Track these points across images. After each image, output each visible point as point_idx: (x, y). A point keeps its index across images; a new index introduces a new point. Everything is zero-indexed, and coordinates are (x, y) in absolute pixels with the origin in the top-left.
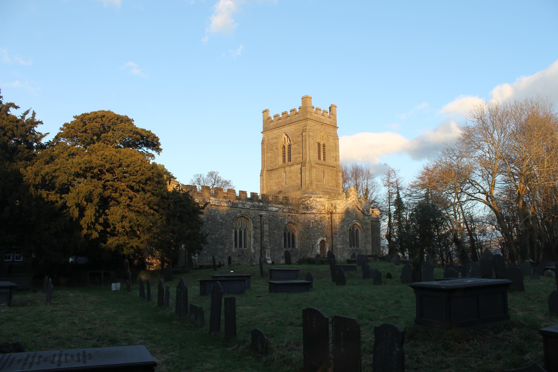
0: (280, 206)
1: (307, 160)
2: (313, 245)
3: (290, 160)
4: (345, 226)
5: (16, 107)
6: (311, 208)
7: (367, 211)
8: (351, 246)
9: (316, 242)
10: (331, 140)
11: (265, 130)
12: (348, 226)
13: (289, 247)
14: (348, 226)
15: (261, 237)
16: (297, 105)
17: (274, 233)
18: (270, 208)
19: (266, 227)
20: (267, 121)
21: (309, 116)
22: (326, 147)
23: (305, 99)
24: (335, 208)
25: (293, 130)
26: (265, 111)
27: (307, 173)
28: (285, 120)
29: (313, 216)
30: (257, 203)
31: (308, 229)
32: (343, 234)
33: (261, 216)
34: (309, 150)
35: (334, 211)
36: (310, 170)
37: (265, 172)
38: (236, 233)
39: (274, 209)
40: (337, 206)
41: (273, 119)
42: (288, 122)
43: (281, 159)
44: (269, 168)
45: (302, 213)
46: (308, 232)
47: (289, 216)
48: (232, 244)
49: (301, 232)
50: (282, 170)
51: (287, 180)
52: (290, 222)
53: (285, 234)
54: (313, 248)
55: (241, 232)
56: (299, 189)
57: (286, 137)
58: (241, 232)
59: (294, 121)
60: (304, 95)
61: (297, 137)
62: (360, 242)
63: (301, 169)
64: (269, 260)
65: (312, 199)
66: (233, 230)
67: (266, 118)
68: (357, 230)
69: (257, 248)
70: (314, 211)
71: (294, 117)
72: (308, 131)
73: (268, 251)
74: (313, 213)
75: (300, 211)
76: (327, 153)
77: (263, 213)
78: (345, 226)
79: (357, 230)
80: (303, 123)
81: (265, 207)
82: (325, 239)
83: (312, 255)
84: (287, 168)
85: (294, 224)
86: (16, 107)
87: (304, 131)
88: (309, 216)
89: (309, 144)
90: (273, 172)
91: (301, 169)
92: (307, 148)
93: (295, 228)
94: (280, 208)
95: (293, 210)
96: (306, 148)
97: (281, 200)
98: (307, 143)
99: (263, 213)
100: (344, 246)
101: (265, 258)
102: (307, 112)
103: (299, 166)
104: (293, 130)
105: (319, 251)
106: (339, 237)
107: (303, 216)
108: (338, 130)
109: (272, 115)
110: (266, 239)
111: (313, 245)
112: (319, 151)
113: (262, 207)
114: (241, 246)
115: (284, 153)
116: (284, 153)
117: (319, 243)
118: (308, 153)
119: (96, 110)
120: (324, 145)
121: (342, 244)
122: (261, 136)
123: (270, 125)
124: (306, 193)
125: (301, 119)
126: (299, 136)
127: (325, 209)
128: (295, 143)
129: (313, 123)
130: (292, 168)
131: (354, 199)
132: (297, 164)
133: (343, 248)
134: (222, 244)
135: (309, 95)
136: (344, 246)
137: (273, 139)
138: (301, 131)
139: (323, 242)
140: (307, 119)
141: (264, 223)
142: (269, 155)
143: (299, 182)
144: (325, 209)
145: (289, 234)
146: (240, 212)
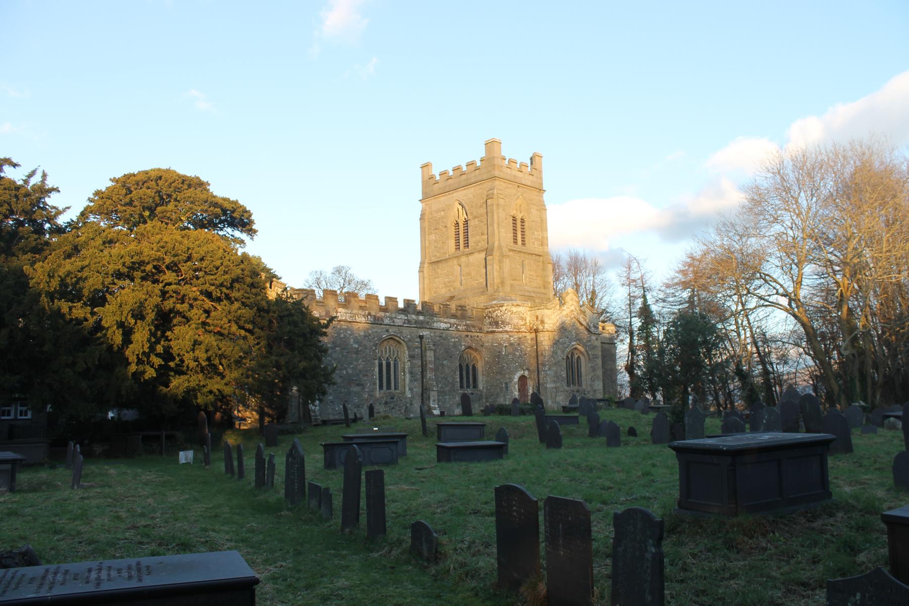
0: (453, 321)
1: (496, 245)
2: (506, 384)
3: (467, 245)
4: (559, 352)
5: (15, 166)
6: (503, 322)
7: (594, 326)
8: (568, 385)
9: (511, 379)
10: (534, 211)
11: (427, 196)
12: (563, 352)
13: (468, 387)
14: (563, 352)
15: (422, 372)
16: (477, 154)
17: (442, 365)
18: (435, 325)
19: (430, 355)
20: (429, 182)
21: (497, 173)
22: (526, 224)
23: (491, 145)
24: (542, 322)
25: (471, 196)
26: (426, 166)
27: (496, 267)
28: (460, 179)
29: (506, 336)
30: (414, 317)
31: (499, 357)
32: (555, 364)
33: (421, 337)
34: (498, 228)
35: (541, 327)
36: (500, 261)
37: (426, 265)
38: (381, 365)
39: (443, 326)
40: (546, 320)
41: (438, 178)
42: (463, 184)
43: (452, 243)
44: (434, 259)
45: (488, 332)
46: (498, 363)
47: (467, 336)
48: (375, 384)
49: (487, 363)
50: (455, 262)
51: (463, 279)
52: (470, 347)
53: (460, 365)
54: (507, 388)
55: (388, 365)
56: (483, 293)
57: (460, 207)
58: (388, 365)
59: (473, 181)
60: (489, 137)
61: (481, 207)
62: (583, 378)
63: (486, 259)
64: (435, 409)
65: (504, 308)
66: (377, 362)
67: (426, 178)
68: (579, 357)
69: (415, 390)
70: (508, 328)
71: (473, 174)
72: (495, 196)
73: (433, 395)
74: (507, 332)
75: (486, 329)
76: (527, 233)
77: (425, 333)
78: (559, 352)
79: (579, 357)
80: (488, 185)
81: (428, 323)
82: (526, 373)
83: (505, 400)
84: (463, 259)
85: (476, 350)
86: (15, 166)
87: (489, 197)
88: (500, 335)
89: (498, 218)
90: (440, 265)
91: (486, 259)
92: (496, 226)
93: (478, 357)
94: (452, 325)
95: (474, 327)
96: (492, 225)
97: (453, 311)
98: (495, 217)
99: (425, 333)
100: (558, 385)
101: (429, 406)
102: (493, 166)
103: (483, 255)
104: (471, 196)
105: (516, 394)
106: (549, 369)
107: (491, 336)
108: (546, 197)
109: (436, 171)
110: (429, 375)
111: (506, 384)
112: (515, 230)
113: (422, 322)
114: (389, 387)
115: (457, 234)
116: (457, 234)
117: (516, 380)
118: (496, 231)
119: (147, 168)
120: (523, 221)
121: (555, 382)
122: (419, 207)
123: (434, 188)
124: (494, 299)
125: (485, 177)
126: (481, 206)
127: (525, 324)
128: (475, 217)
129: (504, 185)
130: (471, 258)
131: (573, 308)
132: (479, 252)
133: (556, 388)
134: (358, 385)
135: (497, 138)
136: (558, 385)
137: (438, 211)
138: (485, 197)
139: (523, 378)
140: (494, 178)
141: (426, 349)
142: (433, 237)
143: (483, 280)
144: (525, 324)
145: (467, 366)
146: (387, 331)
